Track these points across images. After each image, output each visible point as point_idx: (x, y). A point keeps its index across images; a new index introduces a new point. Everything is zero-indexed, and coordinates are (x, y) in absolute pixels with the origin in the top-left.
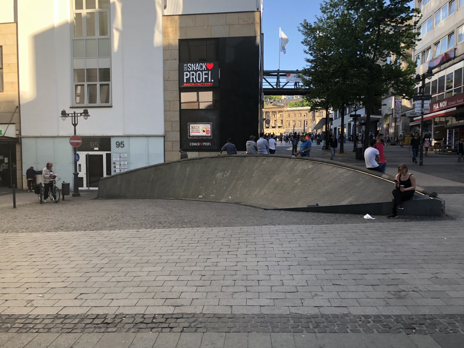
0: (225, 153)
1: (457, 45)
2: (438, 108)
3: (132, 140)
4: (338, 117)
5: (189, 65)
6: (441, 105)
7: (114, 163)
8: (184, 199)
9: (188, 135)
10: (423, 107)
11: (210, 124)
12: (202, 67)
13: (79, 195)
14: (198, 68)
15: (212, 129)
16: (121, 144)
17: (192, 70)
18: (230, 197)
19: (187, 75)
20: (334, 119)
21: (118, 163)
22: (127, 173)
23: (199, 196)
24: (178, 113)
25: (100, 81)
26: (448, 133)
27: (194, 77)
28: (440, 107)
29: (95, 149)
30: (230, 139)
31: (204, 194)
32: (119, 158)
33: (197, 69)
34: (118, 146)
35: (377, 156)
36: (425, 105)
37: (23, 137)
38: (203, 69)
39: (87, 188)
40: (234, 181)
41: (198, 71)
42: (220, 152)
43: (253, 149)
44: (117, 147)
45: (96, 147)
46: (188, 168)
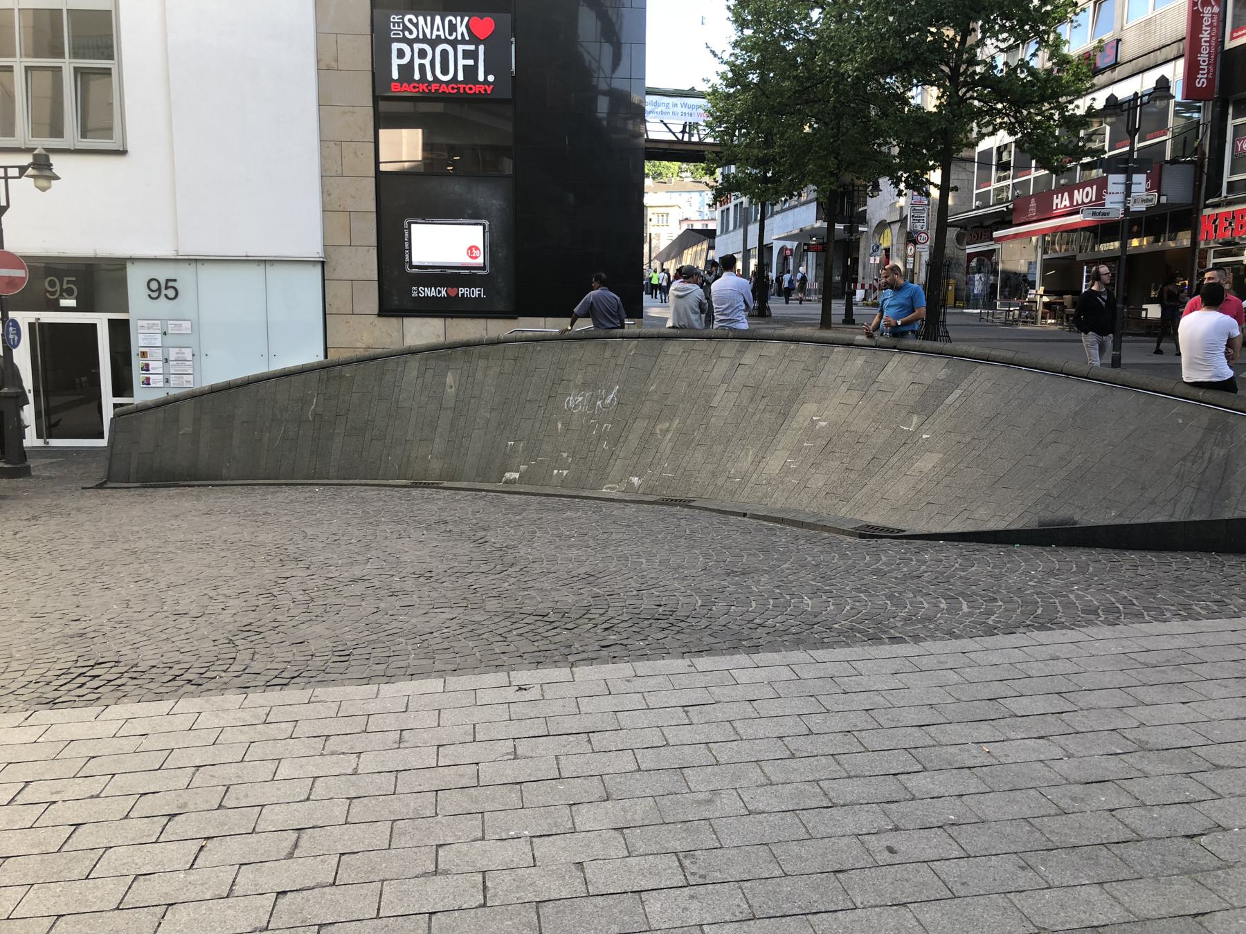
0: (585, 325)
1: (1122, 29)
2: (1068, 205)
3: (206, 272)
4: (731, 227)
5: (410, 21)
6: (1078, 196)
7: (144, 354)
8: (446, 484)
9: (407, 259)
10: (1128, 192)
11: (480, 224)
12: (453, 28)
13: (25, 472)
14: (441, 33)
15: (487, 243)
16: (167, 288)
17: (421, 37)
18: (635, 480)
19: (401, 54)
20: (718, 233)
21: (158, 354)
22: (215, 391)
23: (508, 475)
24: (371, 184)
25: (76, 54)
26: (1085, 274)
27: (427, 62)
28: (1075, 203)
29: (64, 303)
30: (603, 275)
31: (523, 467)
32: (159, 337)
33: (438, 36)
34: (155, 295)
35: (1230, 343)
36: (1134, 188)
37: (601, 47)
38: (459, 38)
39: (39, 443)
40: (641, 424)
41: (439, 40)
42: (569, 320)
43: (695, 313)
44: (149, 296)
45: (69, 293)
46: (450, 374)
